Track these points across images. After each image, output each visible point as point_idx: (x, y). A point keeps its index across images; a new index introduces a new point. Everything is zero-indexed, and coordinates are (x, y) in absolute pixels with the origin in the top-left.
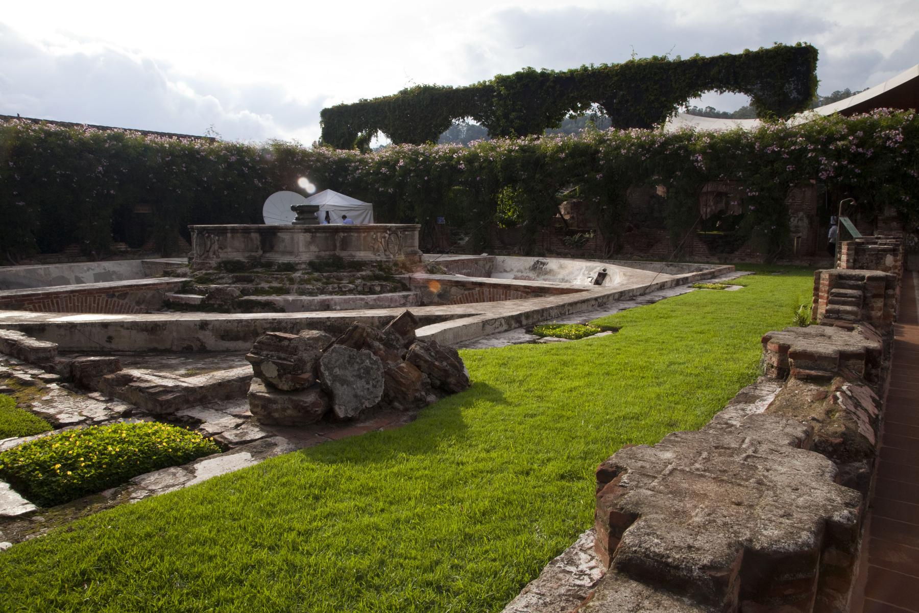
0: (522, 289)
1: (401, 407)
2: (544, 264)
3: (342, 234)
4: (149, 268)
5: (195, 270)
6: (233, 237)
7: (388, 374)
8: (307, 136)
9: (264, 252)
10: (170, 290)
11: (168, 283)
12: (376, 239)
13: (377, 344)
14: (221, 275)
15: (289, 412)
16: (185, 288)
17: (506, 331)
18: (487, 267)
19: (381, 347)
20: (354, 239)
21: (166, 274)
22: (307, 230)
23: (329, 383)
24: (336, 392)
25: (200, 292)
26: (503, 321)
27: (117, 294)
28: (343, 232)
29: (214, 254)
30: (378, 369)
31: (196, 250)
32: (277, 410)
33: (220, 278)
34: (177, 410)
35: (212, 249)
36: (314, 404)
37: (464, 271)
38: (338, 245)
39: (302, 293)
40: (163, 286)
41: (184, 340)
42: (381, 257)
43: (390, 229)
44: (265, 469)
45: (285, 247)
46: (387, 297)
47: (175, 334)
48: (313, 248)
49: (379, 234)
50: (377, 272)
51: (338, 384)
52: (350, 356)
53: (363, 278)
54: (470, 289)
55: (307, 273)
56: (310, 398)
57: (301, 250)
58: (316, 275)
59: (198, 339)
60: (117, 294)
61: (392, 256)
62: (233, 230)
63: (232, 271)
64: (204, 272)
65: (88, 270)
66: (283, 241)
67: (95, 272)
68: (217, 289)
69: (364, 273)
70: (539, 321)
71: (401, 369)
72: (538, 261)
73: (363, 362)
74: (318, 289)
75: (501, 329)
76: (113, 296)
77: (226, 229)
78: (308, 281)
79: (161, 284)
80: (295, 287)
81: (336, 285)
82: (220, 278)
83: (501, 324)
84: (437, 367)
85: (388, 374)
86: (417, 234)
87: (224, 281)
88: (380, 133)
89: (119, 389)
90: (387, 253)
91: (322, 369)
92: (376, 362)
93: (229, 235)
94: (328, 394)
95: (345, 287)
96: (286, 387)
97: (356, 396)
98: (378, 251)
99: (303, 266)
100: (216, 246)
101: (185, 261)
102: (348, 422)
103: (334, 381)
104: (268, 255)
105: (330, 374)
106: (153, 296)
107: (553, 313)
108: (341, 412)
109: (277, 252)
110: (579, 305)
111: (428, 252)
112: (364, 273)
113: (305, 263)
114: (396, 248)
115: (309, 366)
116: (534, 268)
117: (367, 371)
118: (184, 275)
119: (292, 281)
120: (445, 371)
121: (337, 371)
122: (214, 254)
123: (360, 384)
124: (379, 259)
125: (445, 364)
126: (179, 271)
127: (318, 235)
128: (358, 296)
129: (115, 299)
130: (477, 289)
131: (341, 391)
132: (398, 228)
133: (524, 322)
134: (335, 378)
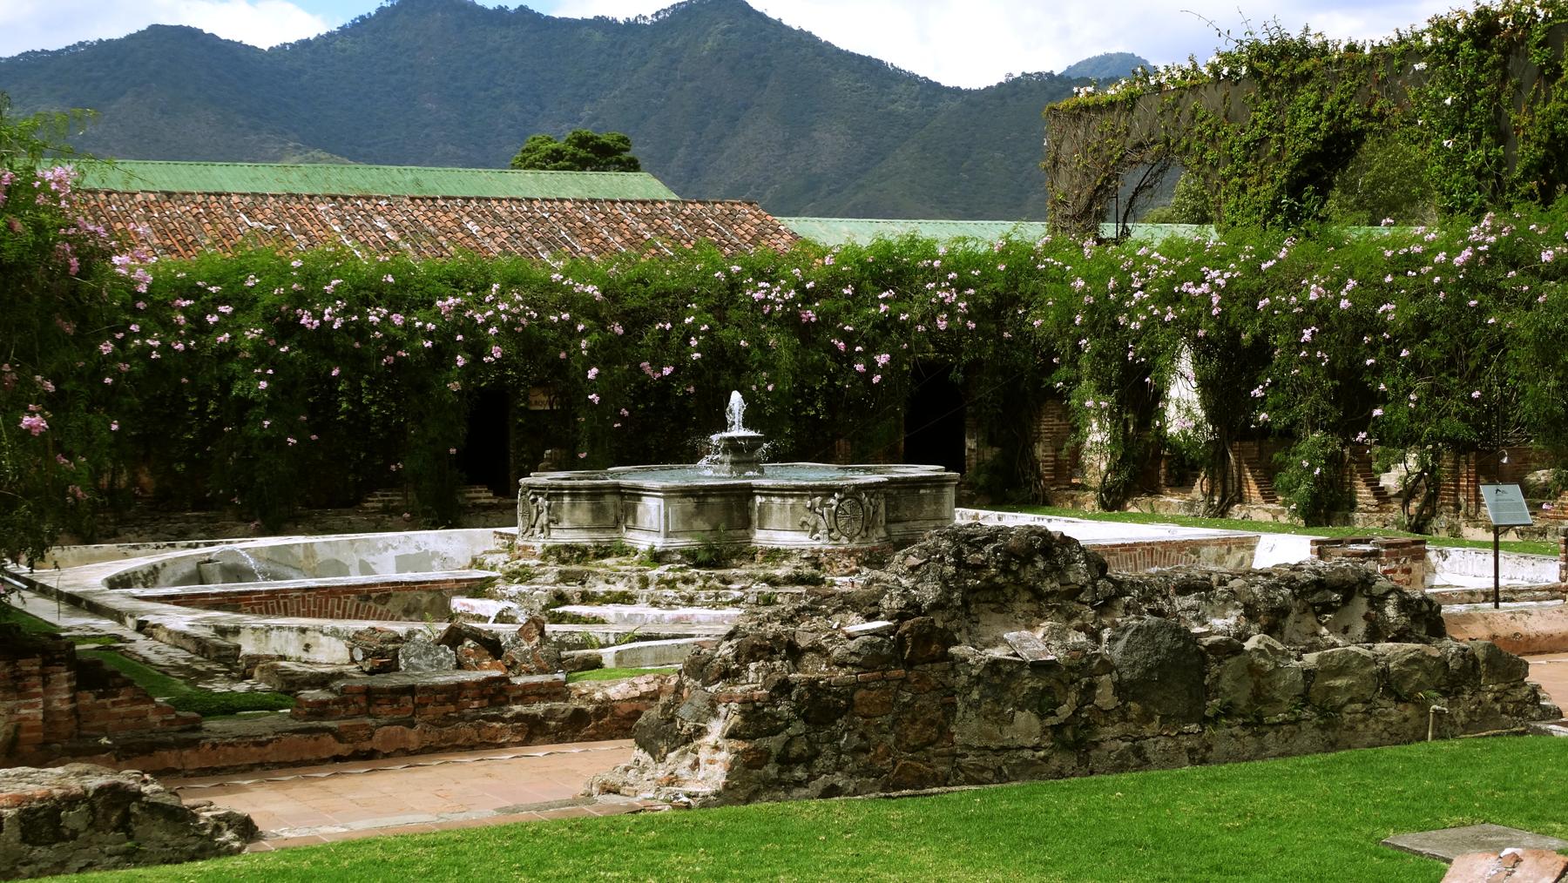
3: (758, 499)
6: (573, 505)
10: (460, 593)
20: (775, 508)
27: (374, 595)
48: (699, 524)
49: (818, 499)
55: (681, 569)
60: (374, 595)
65: (386, 549)
67: (399, 552)
76: (368, 598)
93: (567, 500)
98: (815, 530)
113: (682, 552)
119: (645, 583)
121: (413, 660)
124: (817, 545)
129: (371, 603)
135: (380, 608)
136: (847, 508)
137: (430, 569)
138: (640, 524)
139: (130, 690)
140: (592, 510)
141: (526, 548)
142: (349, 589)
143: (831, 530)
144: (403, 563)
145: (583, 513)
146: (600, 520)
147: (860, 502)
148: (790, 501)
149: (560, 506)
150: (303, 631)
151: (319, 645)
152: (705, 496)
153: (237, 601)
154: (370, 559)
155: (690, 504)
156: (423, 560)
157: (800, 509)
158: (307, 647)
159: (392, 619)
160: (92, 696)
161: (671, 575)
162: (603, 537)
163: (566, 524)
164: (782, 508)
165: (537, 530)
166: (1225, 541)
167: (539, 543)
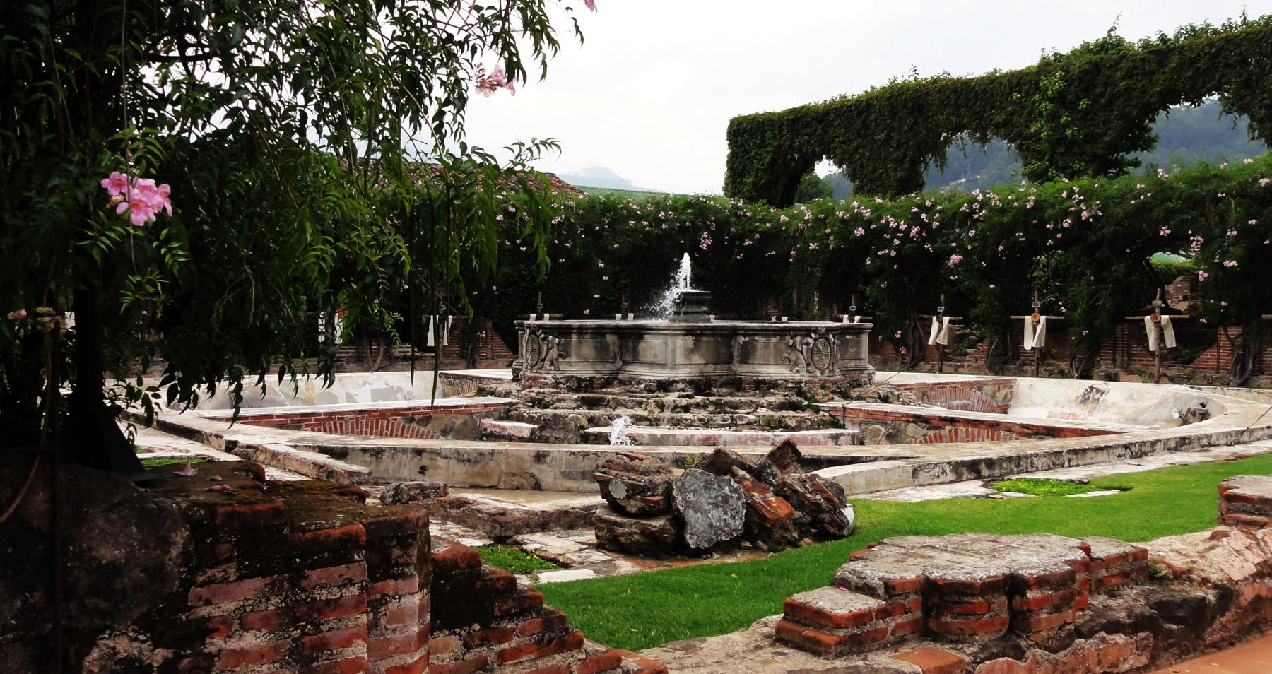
0: (1017, 428)
1: (765, 547)
2: (1101, 392)
3: (742, 339)
4: (450, 384)
5: (524, 388)
6: (580, 342)
7: (751, 508)
8: (697, 169)
9: (626, 363)
10: (487, 416)
11: (486, 406)
12: (793, 347)
13: (742, 472)
14: (560, 396)
15: (636, 537)
16: (507, 413)
17: (952, 482)
18: (1000, 395)
19: (748, 476)
20: (759, 345)
21: (481, 392)
22: (688, 332)
23: (681, 509)
24: (687, 519)
25: (531, 420)
26: (947, 468)
27: (417, 418)
28: (745, 335)
29: (552, 364)
30: (738, 499)
31: (525, 358)
32: (623, 534)
33: (560, 401)
34: (517, 533)
35: (549, 356)
36: (663, 530)
37: (956, 402)
38: (735, 354)
39: (677, 423)
40: (479, 409)
41: (514, 475)
42: (802, 376)
43: (816, 330)
44: (619, 645)
45: (656, 356)
46: (805, 437)
47: (503, 467)
48: (697, 359)
49: (798, 339)
50: (795, 398)
51: (691, 512)
52: (706, 481)
53: (770, 406)
54: (936, 428)
55: (688, 396)
56: (658, 523)
57: (678, 361)
58: (699, 399)
59: (532, 475)
60: (417, 418)
61: (818, 374)
62: (581, 330)
63: (577, 390)
64: (536, 390)
65: (364, 384)
66: (651, 348)
67: (374, 387)
68: (554, 415)
69: (772, 399)
70: (1011, 472)
71: (769, 503)
72: (1092, 388)
73: (721, 488)
74: (701, 420)
75: (943, 479)
76: (412, 420)
77: (570, 327)
78: (686, 409)
79: (476, 406)
80: (668, 414)
81: (727, 416)
82: (560, 401)
83: (944, 472)
84: (807, 499)
85: (751, 508)
86: (865, 339)
87: (564, 404)
88: (825, 161)
89: (453, 512)
90: (810, 369)
91: (675, 492)
92: (736, 491)
93: (574, 337)
94: (679, 522)
95: (741, 418)
96: (633, 510)
97: (711, 526)
98: (796, 364)
99: (681, 386)
100: (554, 353)
101: (507, 374)
102: (698, 553)
103: (686, 507)
104: (629, 368)
105: (684, 499)
106: (465, 423)
107: (1039, 463)
108: (691, 541)
109: (642, 364)
110: (1089, 454)
111: (884, 365)
112: (772, 399)
113: (684, 381)
114: (827, 361)
115: (660, 489)
116: (1085, 400)
117: (726, 500)
118: (507, 394)
119: (661, 406)
120: (819, 505)
121: (691, 497)
122: (552, 364)
123: (716, 513)
124: (797, 377)
125: (819, 497)
126: (501, 388)
127: (705, 339)
128: (760, 433)
129: (414, 425)
130: (948, 428)
131: (691, 516)
132: (829, 330)
133: (985, 472)
134: (688, 505)
135: (422, 429)
136: (820, 346)
137: (397, 399)
138: (643, 359)
139: (534, 622)
140: (596, 347)
141: (535, 379)
142: (396, 412)
143: (808, 365)
144: (377, 395)
145: (588, 348)
146: (602, 355)
147: (828, 340)
148: (774, 340)
149: (568, 343)
150: (418, 452)
151: (437, 468)
152: (701, 335)
153: (300, 421)
154: (352, 392)
155: (690, 340)
156: (391, 393)
157: (783, 346)
158: (423, 470)
159: (432, 438)
160: (455, 642)
161: (684, 401)
162: (607, 369)
163: (574, 359)
164: (767, 346)
165: (547, 364)
166: (997, 382)
167: (549, 375)
